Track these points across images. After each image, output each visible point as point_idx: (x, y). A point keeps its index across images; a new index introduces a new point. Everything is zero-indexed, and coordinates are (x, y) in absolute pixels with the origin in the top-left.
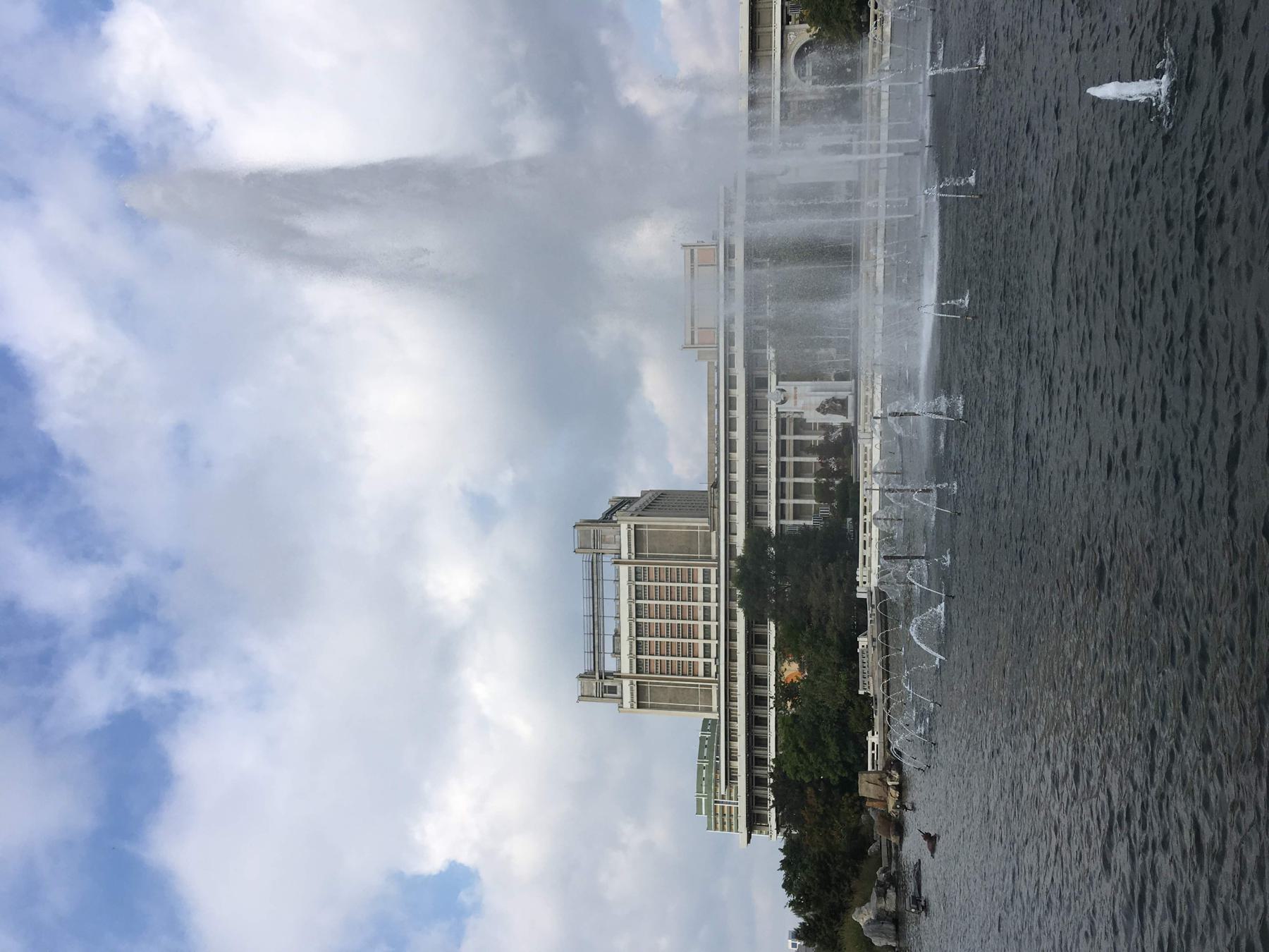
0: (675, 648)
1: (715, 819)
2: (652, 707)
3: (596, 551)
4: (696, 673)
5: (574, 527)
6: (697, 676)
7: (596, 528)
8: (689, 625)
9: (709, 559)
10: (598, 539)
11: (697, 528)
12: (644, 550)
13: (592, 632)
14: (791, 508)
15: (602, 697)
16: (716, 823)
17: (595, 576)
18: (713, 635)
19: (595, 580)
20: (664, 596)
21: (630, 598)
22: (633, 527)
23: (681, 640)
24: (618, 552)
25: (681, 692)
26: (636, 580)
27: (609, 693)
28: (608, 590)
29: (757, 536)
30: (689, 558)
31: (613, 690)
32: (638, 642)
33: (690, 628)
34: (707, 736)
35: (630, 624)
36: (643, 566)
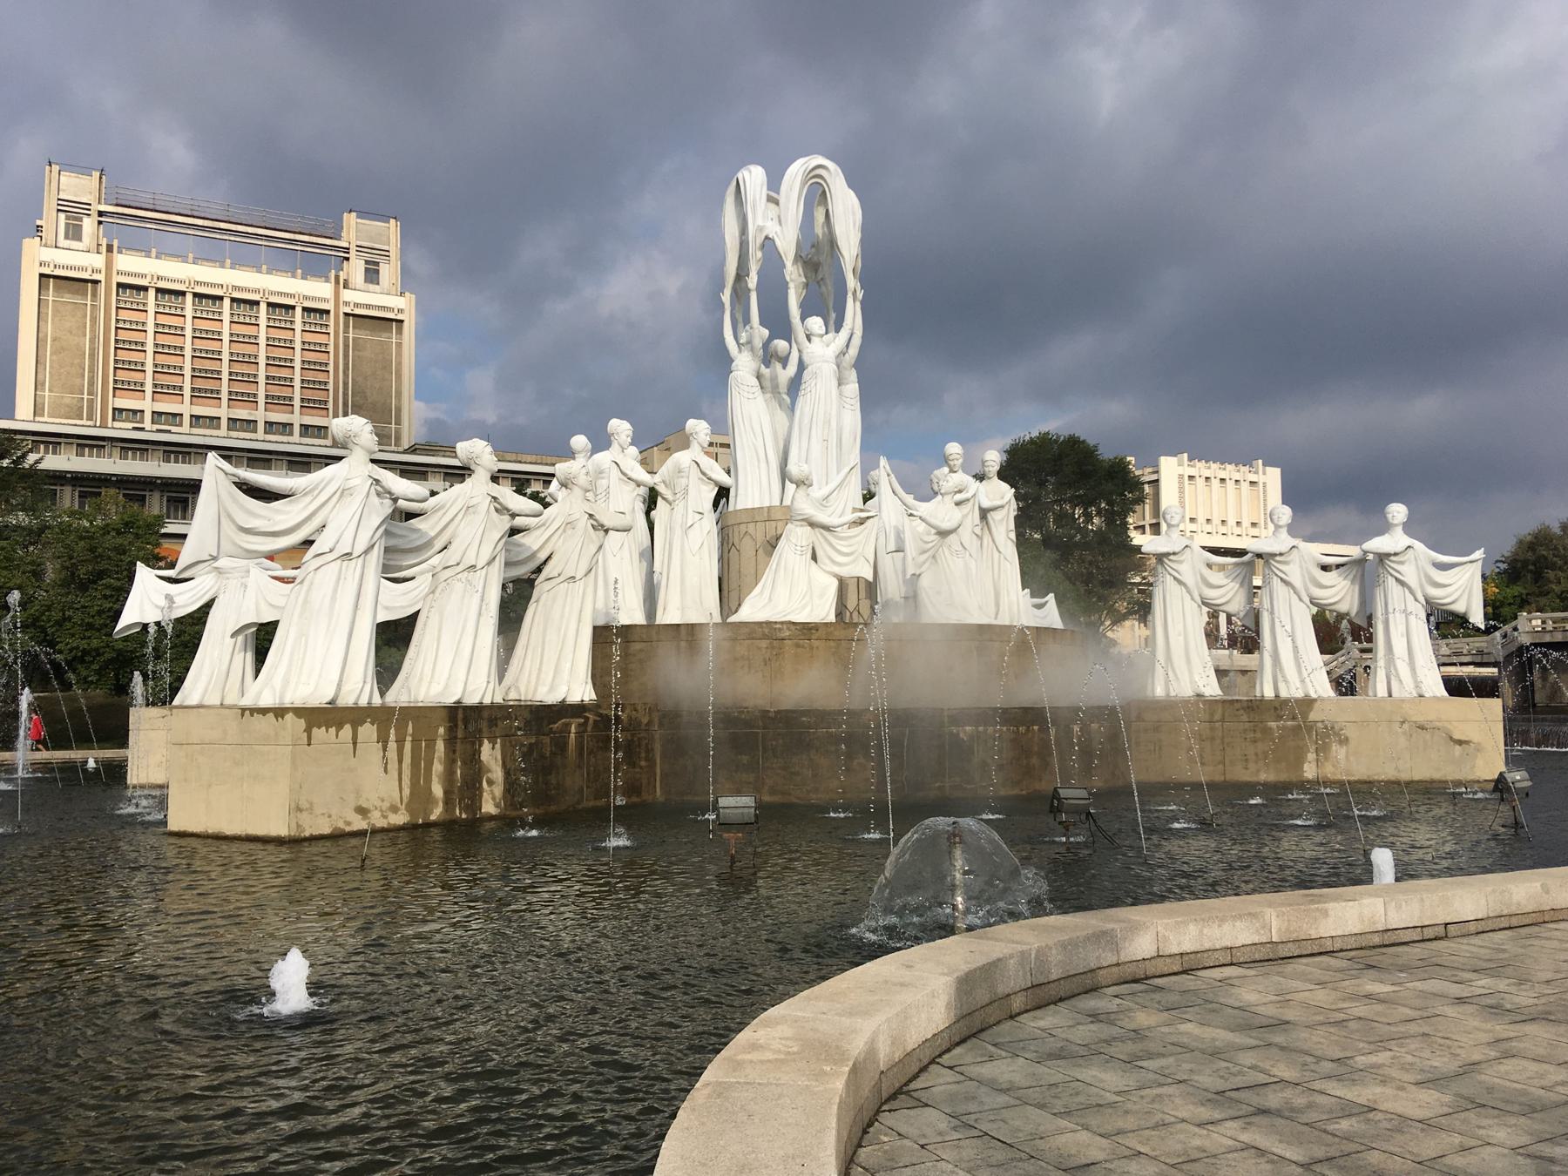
12: (357, 331)
15: (58, 210)
21: (306, 298)
35: (144, 276)
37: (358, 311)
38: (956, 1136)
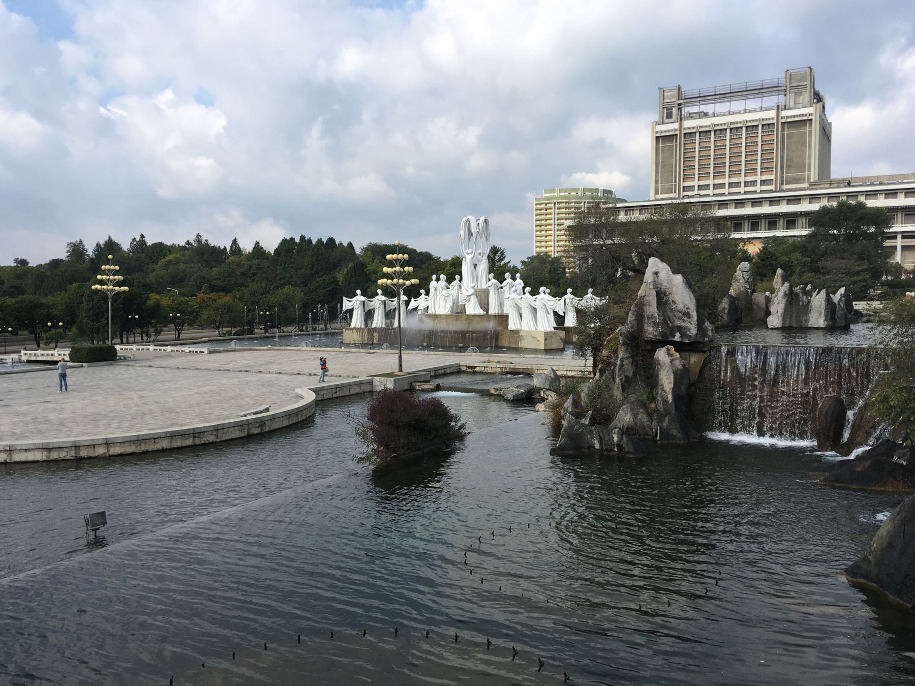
0: (706, 162)
1: (563, 203)
2: (657, 148)
3: (788, 88)
4: (685, 180)
5: (810, 67)
6: (683, 181)
7: (808, 87)
8: (725, 172)
9: (782, 183)
10: (798, 90)
11: (809, 171)
12: (789, 130)
13: (717, 93)
14: (894, 244)
16: (540, 204)
17: (765, 90)
18: (748, 189)
19: (761, 91)
20: (749, 149)
22: (810, 118)
23: (712, 166)
24: (787, 108)
25: (670, 169)
26: (763, 125)
27: (667, 113)
28: (752, 103)
29: (883, 217)
30: (782, 167)
31: (669, 116)
32: (710, 131)
33: (722, 172)
34: (599, 194)
35: (725, 124)
36: (775, 129)
37: (789, 120)
38: (555, 530)
